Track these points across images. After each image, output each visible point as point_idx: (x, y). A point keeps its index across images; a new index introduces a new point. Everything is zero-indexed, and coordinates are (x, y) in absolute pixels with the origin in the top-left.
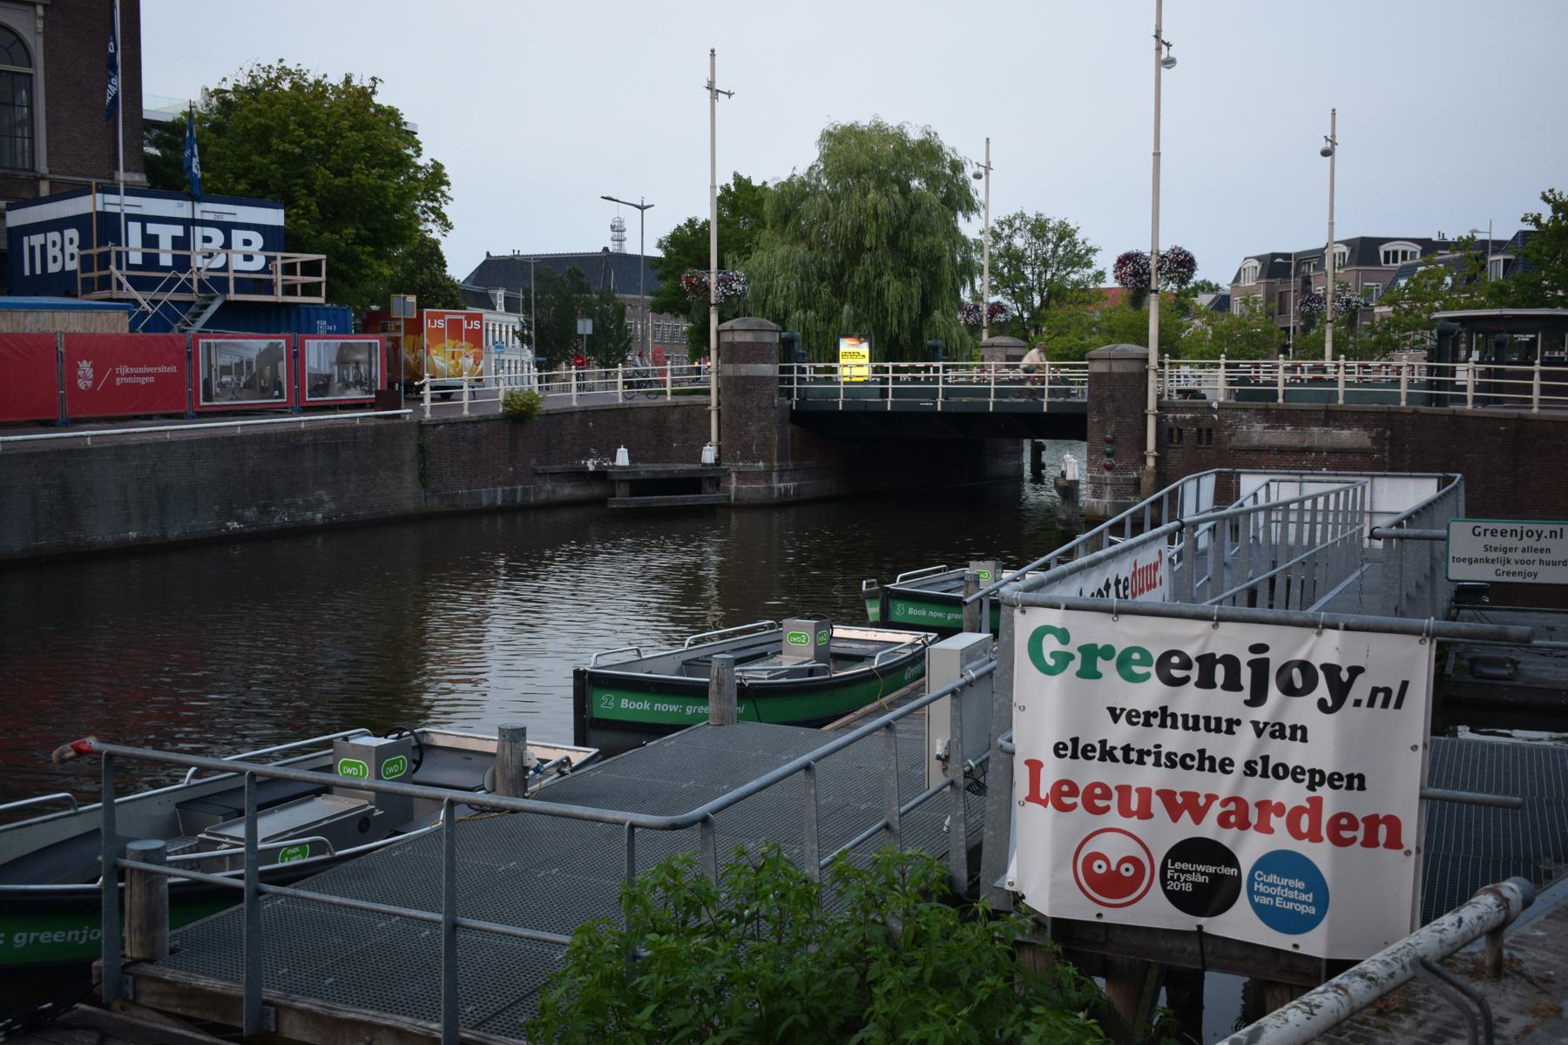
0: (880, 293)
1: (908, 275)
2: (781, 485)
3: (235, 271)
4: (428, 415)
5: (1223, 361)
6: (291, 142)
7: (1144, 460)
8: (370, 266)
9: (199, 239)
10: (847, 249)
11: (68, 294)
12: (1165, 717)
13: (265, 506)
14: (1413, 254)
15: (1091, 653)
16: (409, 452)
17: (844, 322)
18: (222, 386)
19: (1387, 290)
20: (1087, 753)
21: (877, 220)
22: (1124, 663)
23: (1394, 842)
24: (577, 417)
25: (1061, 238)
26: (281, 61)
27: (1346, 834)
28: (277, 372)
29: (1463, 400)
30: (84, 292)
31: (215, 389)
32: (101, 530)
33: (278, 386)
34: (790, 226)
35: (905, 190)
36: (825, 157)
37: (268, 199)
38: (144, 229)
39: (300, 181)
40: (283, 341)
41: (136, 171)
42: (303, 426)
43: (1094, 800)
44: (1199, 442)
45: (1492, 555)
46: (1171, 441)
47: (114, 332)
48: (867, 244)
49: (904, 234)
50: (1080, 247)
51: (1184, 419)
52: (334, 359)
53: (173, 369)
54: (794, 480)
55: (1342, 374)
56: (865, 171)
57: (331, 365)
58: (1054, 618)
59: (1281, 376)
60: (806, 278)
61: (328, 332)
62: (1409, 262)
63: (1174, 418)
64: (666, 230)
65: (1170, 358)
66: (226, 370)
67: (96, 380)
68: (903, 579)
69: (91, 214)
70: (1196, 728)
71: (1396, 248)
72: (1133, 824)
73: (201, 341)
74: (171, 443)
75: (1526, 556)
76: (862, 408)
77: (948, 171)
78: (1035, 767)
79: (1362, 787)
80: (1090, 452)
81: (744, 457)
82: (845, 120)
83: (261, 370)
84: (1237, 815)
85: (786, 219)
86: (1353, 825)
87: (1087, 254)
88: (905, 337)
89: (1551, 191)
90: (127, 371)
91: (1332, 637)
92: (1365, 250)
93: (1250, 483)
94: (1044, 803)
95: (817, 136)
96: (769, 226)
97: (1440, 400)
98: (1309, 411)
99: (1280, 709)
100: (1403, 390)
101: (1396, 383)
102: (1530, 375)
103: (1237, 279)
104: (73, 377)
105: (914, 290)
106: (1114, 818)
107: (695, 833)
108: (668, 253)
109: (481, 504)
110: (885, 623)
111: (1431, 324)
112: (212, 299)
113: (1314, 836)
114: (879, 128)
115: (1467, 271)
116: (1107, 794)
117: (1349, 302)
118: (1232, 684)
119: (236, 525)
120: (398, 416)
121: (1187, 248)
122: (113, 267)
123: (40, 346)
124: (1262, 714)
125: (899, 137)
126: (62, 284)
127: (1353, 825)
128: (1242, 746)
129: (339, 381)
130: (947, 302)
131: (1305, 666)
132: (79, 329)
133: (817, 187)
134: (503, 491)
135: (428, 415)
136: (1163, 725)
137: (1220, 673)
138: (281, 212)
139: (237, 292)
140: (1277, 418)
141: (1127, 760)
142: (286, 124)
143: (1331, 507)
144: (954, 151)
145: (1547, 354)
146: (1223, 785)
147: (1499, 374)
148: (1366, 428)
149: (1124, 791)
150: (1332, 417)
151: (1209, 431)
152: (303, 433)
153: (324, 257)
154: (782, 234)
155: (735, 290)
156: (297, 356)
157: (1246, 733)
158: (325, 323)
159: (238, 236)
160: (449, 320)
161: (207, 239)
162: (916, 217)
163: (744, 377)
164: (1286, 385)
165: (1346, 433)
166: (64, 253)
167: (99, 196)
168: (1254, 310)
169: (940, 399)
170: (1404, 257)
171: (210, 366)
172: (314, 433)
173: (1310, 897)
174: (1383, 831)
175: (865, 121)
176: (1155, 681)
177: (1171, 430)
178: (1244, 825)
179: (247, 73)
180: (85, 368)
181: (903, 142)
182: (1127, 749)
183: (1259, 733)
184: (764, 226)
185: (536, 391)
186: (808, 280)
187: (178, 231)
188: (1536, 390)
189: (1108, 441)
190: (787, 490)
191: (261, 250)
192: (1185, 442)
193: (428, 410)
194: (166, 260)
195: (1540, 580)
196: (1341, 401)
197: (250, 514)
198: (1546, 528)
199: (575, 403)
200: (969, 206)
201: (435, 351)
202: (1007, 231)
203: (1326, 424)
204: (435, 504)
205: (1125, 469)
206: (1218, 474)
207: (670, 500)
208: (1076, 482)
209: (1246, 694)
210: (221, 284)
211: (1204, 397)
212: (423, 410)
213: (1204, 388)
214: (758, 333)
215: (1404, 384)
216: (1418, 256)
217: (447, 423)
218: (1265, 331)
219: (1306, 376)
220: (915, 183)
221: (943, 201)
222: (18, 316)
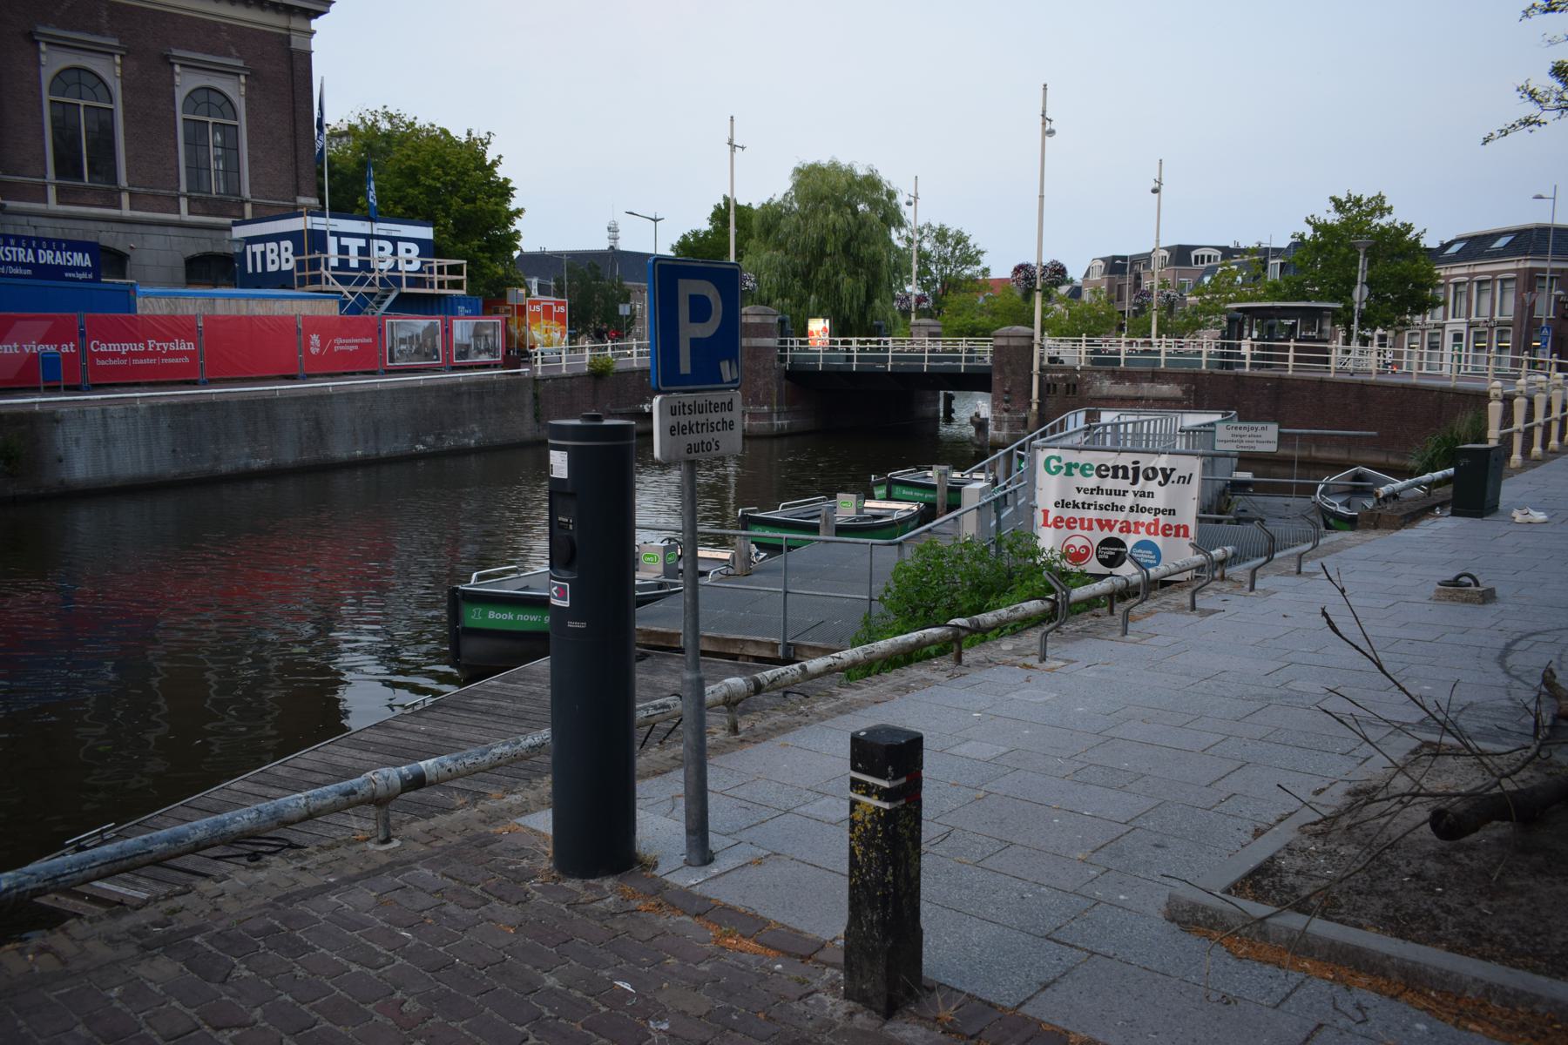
0: (837, 287)
1: (856, 273)
4: (540, 373)
5: (1084, 338)
6: (434, 179)
7: (1030, 405)
8: (489, 268)
9: (376, 249)
10: (813, 254)
11: (283, 287)
12: (1099, 490)
13: (439, 434)
14: (1215, 257)
15: (1069, 466)
16: (528, 398)
17: (811, 308)
18: (401, 352)
19: (1196, 285)
20: (1067, 505)
21: (835, 233)
22: (1083, 470)
23: (1186, 535)
25: (958, 243)
26: (385, 107)
27: (1168, 532)
29: (1243, 365)
30: (299, 286)
31: (396, 355)
32: (341, 449)
33: (436, 352)
34: (771, 237)
35: (855, 213)
36: (797, 186)
37: (417, 219)
38: (339, 241)
39: (440, 206)
40: (439, 321)
41: (311, 197)
43: (1070, 524)
44: (1068, 393)
45: (1235, 439)
46: (1048, 392)
48: (828, 250)
49: (854, 244)
50: (971, 249)
52: (471, 333)
53: (369, 340)
55: (1164, 346)
56: (826, 198)
57: (470, 338)
58: (1055, 452)
59: (1124, 348)
60: (784, 275)
61: (466, 314)
62: (1212, 264)
63: (1051, 377)
64: (676, 239)
66: (403, 341)
67: (322, 348)
68: (784, 507)
69: (303, 231)
70: (1111, 494)
71: (1203, 253)
72: (1085, 533)
74: (381, 391)
75: (1250, 439)
76: (835, 369)
77: (885, 198)
78: (1046, 512)
79: (1174, 514)
80: (994, 400)
81: (753, 403)
82: (809, 160)
83: (425, 340)
84: (1126, 528)
85: (768, 232)
86: (1171, 529)
87: (977, 255)
88: (854, 318)
89: (1312, 216)
91: (1164, 457)
92: (1181, 255)
93: (1107, 417)
94: (1050, 526)
95: (791, 173)
96: (756, 236)
97: (1229, 366)
98: (1141, 373)
99: (1144, 486)
100: (1204, 358)
101: (1200, 353)
102: (1287, 349)
103: (1087, 274)
104: (308, 346)
105: (861, 284)
106: (1078, 531)
107: (896, 547)
108: (678, 255)
110: (889, 498)
111: (1225, 311)
112: (391, 291)
113: (1156, 533)
114: (835, 166)
115: (1254, 272)
116: (1075, 521)
117: (1168, 296)
118: (1125, 477)
120: (518, 373)
121: (1061, 261)
122: (322, 269)
123: (284, 325)
124: (1137, 488)
125: (850, 173)
126: (282, 280)
127: (1171, 529)
128: (1129, 500)
130: (884, 293)
131: (1153, 469)
132: (308, 313)
133: (790, 208)
135: (540, 373)
136: (1098, 493)
137: (1121, 472)
138: (431, 230)
139: (408, 286)
140: (1120, 377)
141: (1083, 508)
142: (428, 166)
143: (1152, 432)
144: (889, 183)
145: (1303, 334)
146: (1121, 516)
147: (1270, 348)
148: (1179, 384)
149: (1082, 520)
150: (1156, 376)
151: (1074, 386)
152: (460, 385)
153: (465, 262)
154: (765, 243)
156: (448, 331)
157: (1130, 496)
159: (402, 246)
161: (382, 249)
162: (864, 231)
164: (1126, 354)
165: (1165, 387)
166: (283, 258)
167: (308, 218)
168: (1100, 299)
169: (890, 363)
170: (1209, 261)
171: (393, 338)
172: (468, 384)
173: (1154, 557)
174: (1182, 531)
175: (825, 161)
176: (1095, 476)
177: (1049, 385)
178: (1129, 531)
179: (357, 114)
180: (315, 339)
181: (853, 177)
182: (1083, 504)
183: (1135, 495)
184: (751, 236)
185: (610, 355)
187: (362, 242)
189: (1007, 392)
190: (783, 425)
193: (540, 369)
194: (354, 263)
195: (1257, 450)
196: (1162, 366)
197: (430, 439)
198: (1259, 425)
199: (635, 365)
200: (901, 223)
202: (918, 237)
203: (1152, 381)
205: (1017, 411)
206: (1087, 411)
208: (987, 419)
209: (1131, 480)
210: (397, 281)
211: (1062, 362)
212: (536, 369)
213: (1062, 356)
215: (1204, 354)
216: (1219, 259)
217: (554, 379)
218: (1107, 314)
219: (1140, 348)
220: (861, 207)
221: (882, 218)
222: (270, 303)
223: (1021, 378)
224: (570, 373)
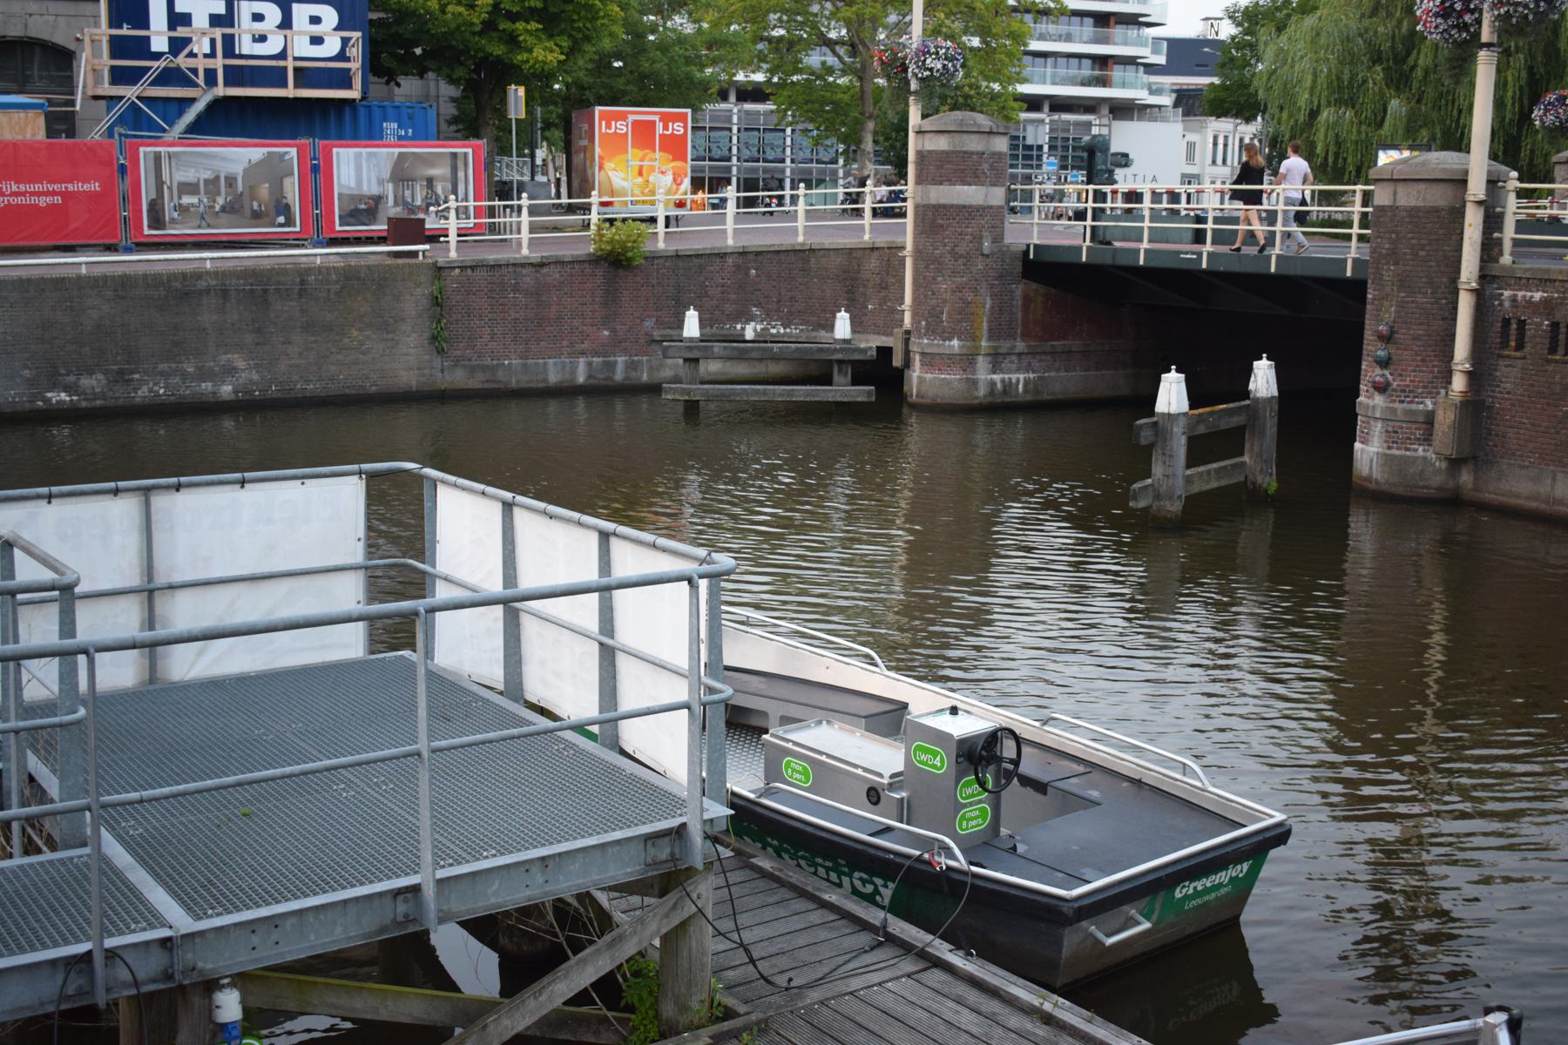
2: (997, 377)
3: (295, 59)
13: (121, 372)
18: (183, 210)
24: (730, 260)
28: (282, 190)
31: (169, 213)
33: (286, 210)
42: (208, 265)
44: (1553, 349)
46: (1504, 344)
47: (20, 137)
51: (1529, 302)
52: (387, 174)
54: (1029, 368)
57: (381, 182)
60: (1348, 58)
61: (400, 138)
63: (1514, 299)
65: (1521, 179)
66: (189, 188)
73: (142, 149)
90: (14, 188)
109: (545, 380)
119: (64, 396)
120: (414, 254)
129: (396, 204)
134: (589, 364)
155: (931, 70)
156: (318, 173)
158: (396, 125)
160: (635, 123)
163: (934, 206)
177: (1506, 323)
186: (1352, 63)
191: (335, 29)
192: (1528, 348)
197: (92, 382)
201: (613, 166)
204: (457, 378)
205: (1407, 393)
206: (372, 478)
207: (765, 392)
214: (957, 137)
223: (1420, 299)
224: (536, 256)
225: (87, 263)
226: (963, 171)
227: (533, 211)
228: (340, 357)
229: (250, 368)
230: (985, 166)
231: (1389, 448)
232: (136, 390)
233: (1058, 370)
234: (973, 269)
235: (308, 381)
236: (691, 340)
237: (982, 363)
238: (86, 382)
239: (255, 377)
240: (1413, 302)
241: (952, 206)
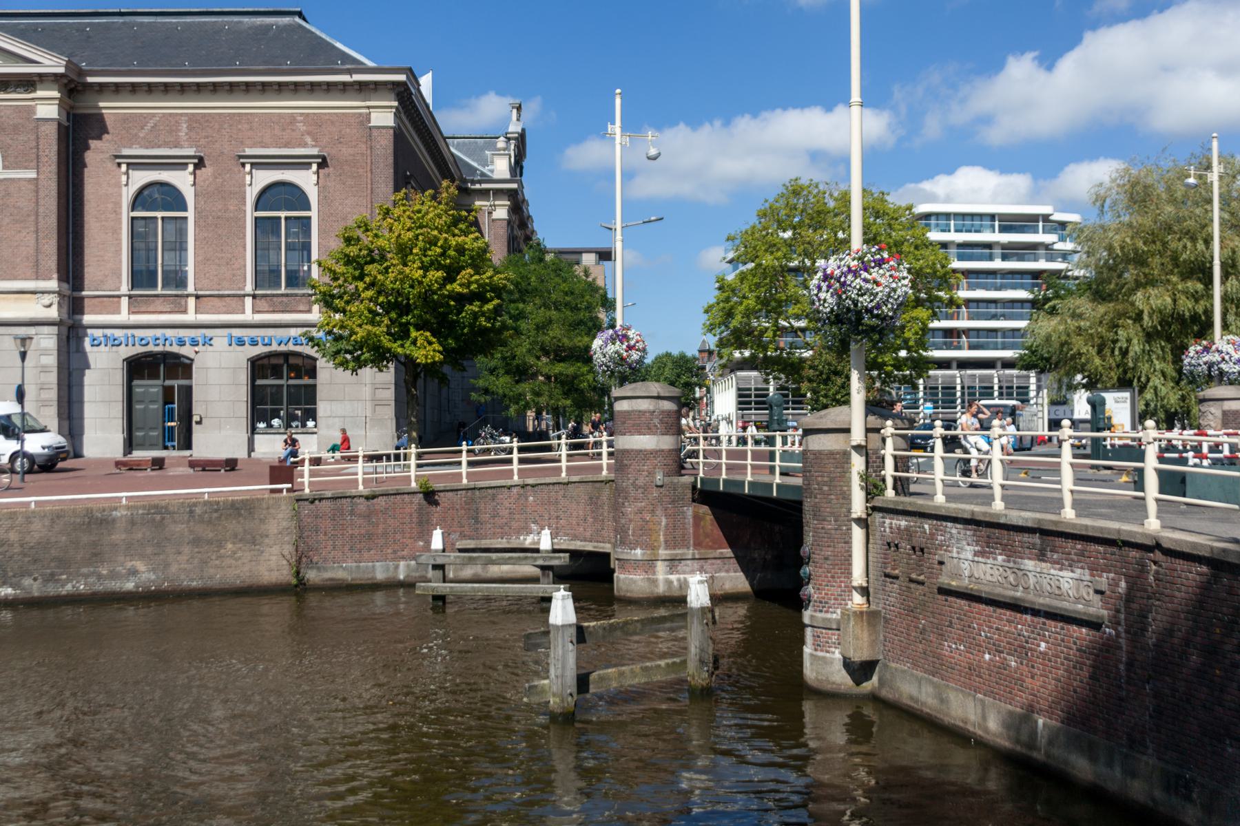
2: (673, 577)
13: (52, 575)
134: (408, 566)
188: (515, 461)
225: (208, 493)
226: (639, 425)
227: (521, 450)
228: (217, 562)
229: (149, 571)
230: (656, 421)
231: (816, 650)
232: (63, 586)
233: (727, 571)
234: (650, 496)
235: (192, 580)
236: (436, 551)
237: (661, 567)
238: (27, 582)
239: (153, 577)
240: (823, 528)
241: (632, 450)
